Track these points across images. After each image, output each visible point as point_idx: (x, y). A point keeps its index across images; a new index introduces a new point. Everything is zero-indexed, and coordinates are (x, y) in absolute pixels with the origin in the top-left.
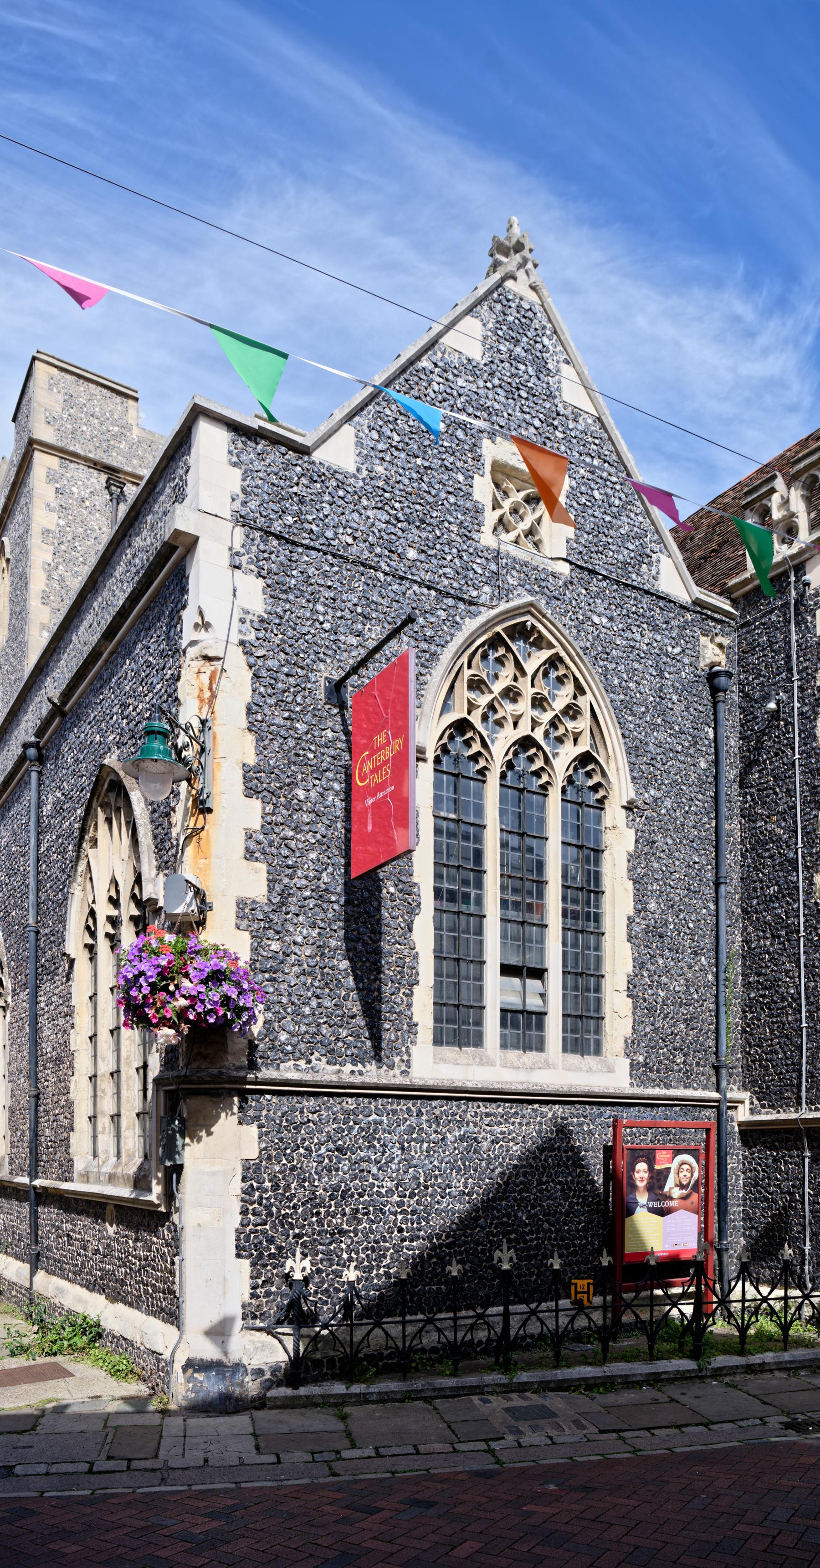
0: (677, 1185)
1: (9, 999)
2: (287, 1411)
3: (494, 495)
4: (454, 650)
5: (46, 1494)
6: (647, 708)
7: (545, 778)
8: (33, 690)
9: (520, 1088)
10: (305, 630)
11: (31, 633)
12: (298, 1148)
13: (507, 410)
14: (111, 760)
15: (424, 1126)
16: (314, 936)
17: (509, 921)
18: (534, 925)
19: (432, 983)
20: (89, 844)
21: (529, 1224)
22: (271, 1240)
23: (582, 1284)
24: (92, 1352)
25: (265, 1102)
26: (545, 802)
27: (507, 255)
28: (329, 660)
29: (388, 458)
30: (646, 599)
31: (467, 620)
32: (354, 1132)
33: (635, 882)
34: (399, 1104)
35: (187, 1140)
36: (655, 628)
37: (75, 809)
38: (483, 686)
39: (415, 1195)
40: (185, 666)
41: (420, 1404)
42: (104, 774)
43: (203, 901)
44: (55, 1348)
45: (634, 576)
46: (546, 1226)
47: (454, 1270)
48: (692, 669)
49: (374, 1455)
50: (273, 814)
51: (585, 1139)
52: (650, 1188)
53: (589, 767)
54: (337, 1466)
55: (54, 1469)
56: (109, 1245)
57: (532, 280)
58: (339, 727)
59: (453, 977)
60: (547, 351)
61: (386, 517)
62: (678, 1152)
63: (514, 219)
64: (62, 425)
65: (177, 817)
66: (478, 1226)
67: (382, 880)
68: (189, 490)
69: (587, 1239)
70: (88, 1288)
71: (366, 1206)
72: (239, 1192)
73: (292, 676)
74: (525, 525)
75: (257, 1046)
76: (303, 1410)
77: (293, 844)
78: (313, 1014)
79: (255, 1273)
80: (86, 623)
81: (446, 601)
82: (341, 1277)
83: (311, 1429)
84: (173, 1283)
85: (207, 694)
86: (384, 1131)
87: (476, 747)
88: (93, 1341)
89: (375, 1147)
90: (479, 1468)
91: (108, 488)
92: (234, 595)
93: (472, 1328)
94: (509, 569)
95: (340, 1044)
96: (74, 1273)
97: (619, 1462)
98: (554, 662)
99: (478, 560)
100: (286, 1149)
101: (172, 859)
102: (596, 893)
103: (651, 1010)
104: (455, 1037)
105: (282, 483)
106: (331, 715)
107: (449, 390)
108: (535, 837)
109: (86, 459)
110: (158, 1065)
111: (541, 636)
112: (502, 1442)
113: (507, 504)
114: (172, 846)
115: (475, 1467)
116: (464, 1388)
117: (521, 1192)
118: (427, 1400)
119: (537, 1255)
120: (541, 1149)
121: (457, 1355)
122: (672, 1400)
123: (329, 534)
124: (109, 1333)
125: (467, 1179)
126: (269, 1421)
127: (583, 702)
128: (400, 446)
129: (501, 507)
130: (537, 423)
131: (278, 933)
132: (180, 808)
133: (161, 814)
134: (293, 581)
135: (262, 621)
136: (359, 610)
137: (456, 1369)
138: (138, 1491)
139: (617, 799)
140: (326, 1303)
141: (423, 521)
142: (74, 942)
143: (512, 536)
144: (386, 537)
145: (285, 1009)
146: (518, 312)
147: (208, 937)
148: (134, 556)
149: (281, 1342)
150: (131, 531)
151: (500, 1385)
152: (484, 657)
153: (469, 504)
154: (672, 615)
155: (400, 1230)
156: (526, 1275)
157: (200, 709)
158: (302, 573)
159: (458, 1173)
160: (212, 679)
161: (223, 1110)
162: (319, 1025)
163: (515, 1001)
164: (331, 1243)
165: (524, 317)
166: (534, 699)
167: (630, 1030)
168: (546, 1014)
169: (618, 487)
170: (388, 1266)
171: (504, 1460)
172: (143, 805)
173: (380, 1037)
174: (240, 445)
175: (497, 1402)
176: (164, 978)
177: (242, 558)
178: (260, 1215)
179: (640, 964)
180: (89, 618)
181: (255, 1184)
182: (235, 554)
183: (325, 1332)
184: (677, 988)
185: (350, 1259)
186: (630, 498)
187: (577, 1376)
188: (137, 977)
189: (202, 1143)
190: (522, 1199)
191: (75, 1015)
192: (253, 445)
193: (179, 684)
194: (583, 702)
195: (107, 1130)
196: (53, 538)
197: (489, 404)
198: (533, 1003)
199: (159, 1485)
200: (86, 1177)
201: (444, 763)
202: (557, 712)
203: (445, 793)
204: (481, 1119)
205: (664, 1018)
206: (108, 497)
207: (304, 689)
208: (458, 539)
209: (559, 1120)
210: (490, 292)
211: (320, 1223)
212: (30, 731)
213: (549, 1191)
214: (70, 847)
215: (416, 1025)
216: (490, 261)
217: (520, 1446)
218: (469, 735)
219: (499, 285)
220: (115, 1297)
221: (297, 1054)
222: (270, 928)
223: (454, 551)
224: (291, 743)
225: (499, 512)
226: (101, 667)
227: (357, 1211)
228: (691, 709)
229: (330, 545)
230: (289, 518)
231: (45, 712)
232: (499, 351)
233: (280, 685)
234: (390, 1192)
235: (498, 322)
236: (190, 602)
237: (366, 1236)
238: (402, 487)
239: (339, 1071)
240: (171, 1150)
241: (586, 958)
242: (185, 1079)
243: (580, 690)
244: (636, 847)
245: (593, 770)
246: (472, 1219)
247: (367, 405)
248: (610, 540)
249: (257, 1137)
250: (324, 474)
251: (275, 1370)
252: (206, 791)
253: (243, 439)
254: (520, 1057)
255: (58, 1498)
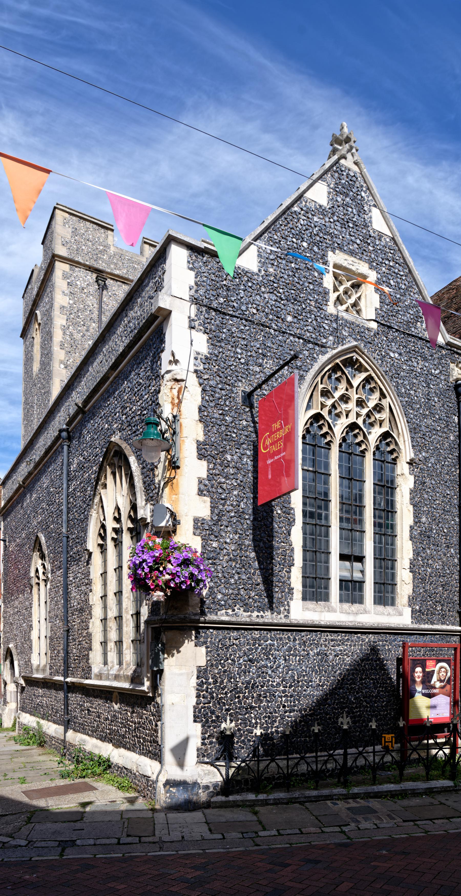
0: (438, 680)
1: (49, 575)
2: (222, 810)
3: (334, 284)
4: (313, 373)
5: (97, 856)
6: (421, 405)
7: (363, 447)
8: (64, 399)
9: (351, 625)
10: (230, 363)
11: (54, 365)
12: (228, 660)
13: (341, 235)
14: (115, 439)
15: (297, 647)
16: (236, 539)
17: (344, 529)
18: (358, 531)
19: (301, 565)
20: (101, 487)
21: (355, 703)
22: (213, 712)
23: (388, 737)
24: (105, 776)
25: (209, 634)
26: (363, 461)
27: (340, 145)
28: (244, 381)
29: (276, 264)
30: (420, 343)
31: (320, 356)
32: (259, 651)
33: (414, 506)
34: (283, 634)
35: (166, 656)
36: (425, 359)
37: (92, 467)
38: (329, 394)
39: (292, 686)
40: (163, 385)
41: (297, 805)
42: (111, 447)
43: (175, 519)
44: (84, 774)
45: (413, 329)
46: (364, 704)
47: (316, 729)
48: (446, 382)
49: (277, 834)
50: (214, 469)
51: (386, 654)
52: (423, 682)
53: (388, 440)
54: (258, 840)
55: (98, 842)
56: (115, 715)
57: (355, 159)
58: (250, 419)
59: (312, 561)
60: (364, 200)
61: (275, 298)
62: (439, 661)
63: (345, 124)
64: (71, 246)
65: (159, 471)
66: (327, 704)
67: (274, 506)
68: (165, 284)
69: (387, 711)
70: (101, 740)
71: (265, 692)
72: (195, 685)
73: (224, 390)
74: (352, 301)
75: (205, 602)
76: (231, 809)
77: (224, 486)
78: (236, 583)
79: (204, 731)
80: (98, 360)
81: (308, 345)
82: (252, 733)
83: (238, 820)
84: (157, 737)
85: (176, 401)
86: (275, 650)
87: (325, 429)
88: (105, 770)
89: (270, 659)
90: (339, 841)
91: (97, 281)
92: (191, 344)
93: (326, 762)
94: (343, 326)
95: (251, 600)
96: (92, 731)
97: (419, 838)
98: (368, 380)
99: (326, 322)
100: (221, 660)
101: (156, 495)
102: (392, 512)
103: (423, 580)
104: (313, 596)
105: (217, 279)
106: (245, 412)
107: (309, 224)
108: (358, 481)
109: (84, 265)
110: (147, 613)
111: (361, 365)
112: (349, 827)
113: (341, 289)
114: (156, 488)
115: (337, 841)
116: (322, 796)
117: (351, 684)
118: (301, 803)
119: (360, 720)
120: (362, 660)
121: (317, 777)
122: (441, 803)
123: (244, 308)
124: (116, 765)
125: (321, 677)
126: (214, 815)
127: (385, 403)
128: (283, 256)
129: (338, 291)
130: (358, 241)
131: (216, 537)
132: (161, 466)
133: (149, 470)
134: (224, 336)
135: (207, 358)
136: (260, 351)
137: (317, 786)
138: (149, 854)
139: (404, 458)
140: (243, 748)
141: (295, 300)
142: (92, 543)
143: (344, 307)
144: (275, 309)
145: (220, 581)
146: (347, 178)
147: (179, 539)
148: (129, 322)
149: (218, 770)
150: (127, 308)
151: (342, 795)
152: (330, 377)
153: (321, 290)
154: (434, 351)
155: (284, 706)
156: (354, 732)
157: (172, 409)
158: (229, 330)
159: (316, 674)
160: (179, 392)
161: (186, 638)
162: (239, 589)
163: (347, 575)
164: (246, 714)
165: (351, 180)
166: (357, 401)
167: (411, 591)
168: (364, 582)
169: (404, 278)
170: (277, 727)
171: (352, 837)
172: (136, 464)
173: (273, 596)
174: (194, 258)
175: (341, 805)
176: (157, 563)
177: (196, 323)
178: (207, 698)
179: (417, 553)
180: (100, 357)
181: (204, 680)
182: (191, 320)
183: (243, 765)
184: (438, 567)
185: (256, 723)
186: (411, 284)
187: (386, 790)
188: (141, 563)
189: (174, 658)
190: (352, 688)
191: (93, 584)
192: (201, 258)
193: (160, 395)
194: (385, 403)
195: (113, 650)
196: (67, 311)
197: (331, 231)
198: (357, 576)
199: (160, 851)
200: (100, 676)
201: (307, 438)
202: (370, 408)
203: (308, 456)
204: (329, 643)
205: (430, 584)
206: (97, 287)
207: (230, 397)
208: (315, 309)
209: (372, 643)
210: (332, 166)
211: (240, 702)
212: (62, 422)
213: (366, 684)
214: (89, 489)
215: (293, 589)
216: (331, 148)
217: (359, 829)
218: (321, 422)
219: (337, 162)
220: (118, 745)
221: (227, 606)
222: (212, 534)
223: (313, 316)
224: (223, 428)
225: (337, 294)
226: (108, 386)
227: (260, 695)
228: (445, 406)
229: (244, 314)
230: (221, 299)
231: (72, 411)
232: (337, 201)
233: (217, 395)
234: (278, 684)
235: (336, 184)
236: (166, 348)
237: (265, 709)
238: (284, 280)
239: (250, 616)
240: (157, 661)
241: (386, 549)
242: (165, 621)
243: (383, 396)
244: (415, 486)
245: (390, 442)
246: (324, 700)
247: (264, 233)
248: (400, 309)
249: (205, 653)
250: (240, 274)
251: (215, 786)
252: (176, 456)
253: (196, 254)
254: (350, 607)
255: (105, 858)
